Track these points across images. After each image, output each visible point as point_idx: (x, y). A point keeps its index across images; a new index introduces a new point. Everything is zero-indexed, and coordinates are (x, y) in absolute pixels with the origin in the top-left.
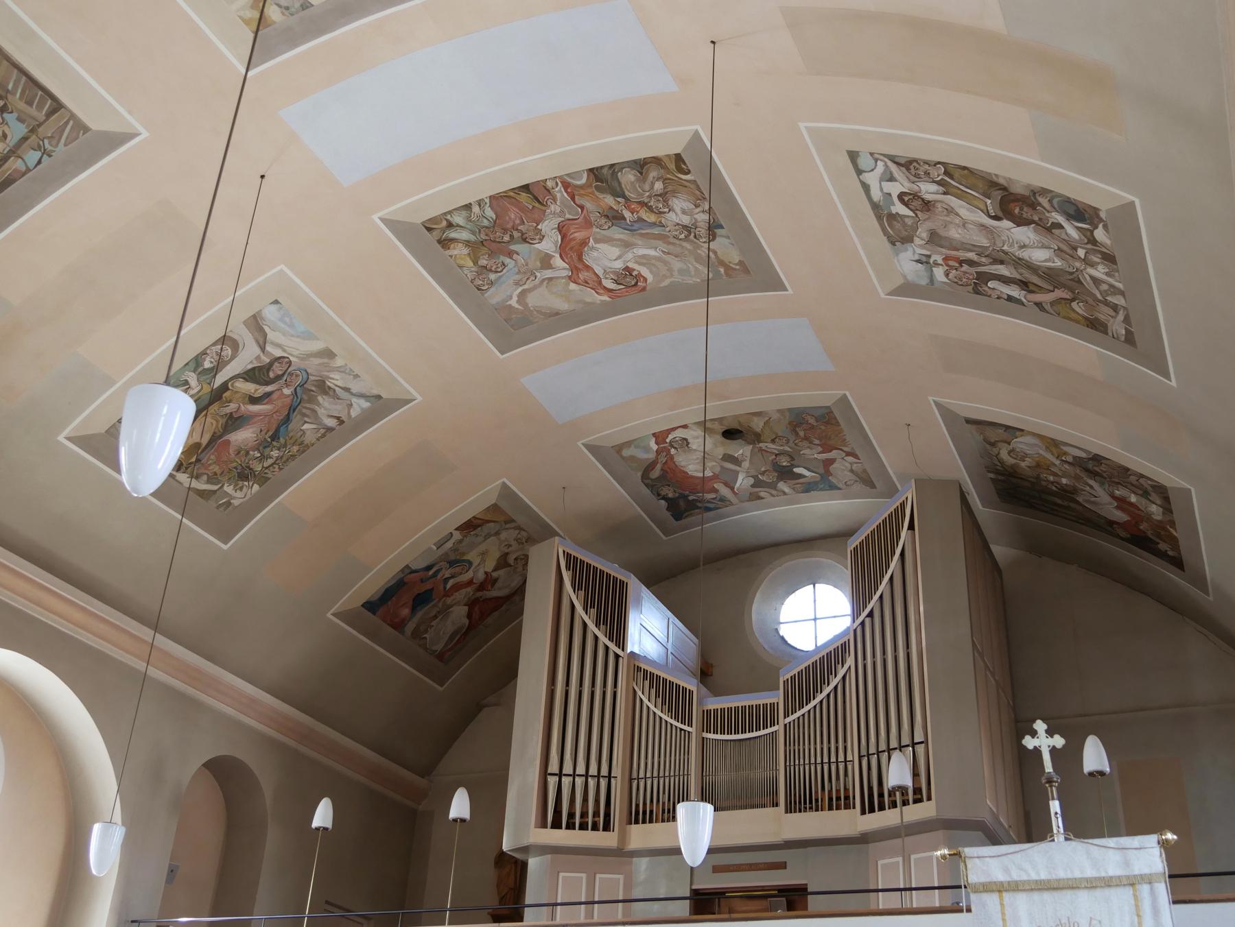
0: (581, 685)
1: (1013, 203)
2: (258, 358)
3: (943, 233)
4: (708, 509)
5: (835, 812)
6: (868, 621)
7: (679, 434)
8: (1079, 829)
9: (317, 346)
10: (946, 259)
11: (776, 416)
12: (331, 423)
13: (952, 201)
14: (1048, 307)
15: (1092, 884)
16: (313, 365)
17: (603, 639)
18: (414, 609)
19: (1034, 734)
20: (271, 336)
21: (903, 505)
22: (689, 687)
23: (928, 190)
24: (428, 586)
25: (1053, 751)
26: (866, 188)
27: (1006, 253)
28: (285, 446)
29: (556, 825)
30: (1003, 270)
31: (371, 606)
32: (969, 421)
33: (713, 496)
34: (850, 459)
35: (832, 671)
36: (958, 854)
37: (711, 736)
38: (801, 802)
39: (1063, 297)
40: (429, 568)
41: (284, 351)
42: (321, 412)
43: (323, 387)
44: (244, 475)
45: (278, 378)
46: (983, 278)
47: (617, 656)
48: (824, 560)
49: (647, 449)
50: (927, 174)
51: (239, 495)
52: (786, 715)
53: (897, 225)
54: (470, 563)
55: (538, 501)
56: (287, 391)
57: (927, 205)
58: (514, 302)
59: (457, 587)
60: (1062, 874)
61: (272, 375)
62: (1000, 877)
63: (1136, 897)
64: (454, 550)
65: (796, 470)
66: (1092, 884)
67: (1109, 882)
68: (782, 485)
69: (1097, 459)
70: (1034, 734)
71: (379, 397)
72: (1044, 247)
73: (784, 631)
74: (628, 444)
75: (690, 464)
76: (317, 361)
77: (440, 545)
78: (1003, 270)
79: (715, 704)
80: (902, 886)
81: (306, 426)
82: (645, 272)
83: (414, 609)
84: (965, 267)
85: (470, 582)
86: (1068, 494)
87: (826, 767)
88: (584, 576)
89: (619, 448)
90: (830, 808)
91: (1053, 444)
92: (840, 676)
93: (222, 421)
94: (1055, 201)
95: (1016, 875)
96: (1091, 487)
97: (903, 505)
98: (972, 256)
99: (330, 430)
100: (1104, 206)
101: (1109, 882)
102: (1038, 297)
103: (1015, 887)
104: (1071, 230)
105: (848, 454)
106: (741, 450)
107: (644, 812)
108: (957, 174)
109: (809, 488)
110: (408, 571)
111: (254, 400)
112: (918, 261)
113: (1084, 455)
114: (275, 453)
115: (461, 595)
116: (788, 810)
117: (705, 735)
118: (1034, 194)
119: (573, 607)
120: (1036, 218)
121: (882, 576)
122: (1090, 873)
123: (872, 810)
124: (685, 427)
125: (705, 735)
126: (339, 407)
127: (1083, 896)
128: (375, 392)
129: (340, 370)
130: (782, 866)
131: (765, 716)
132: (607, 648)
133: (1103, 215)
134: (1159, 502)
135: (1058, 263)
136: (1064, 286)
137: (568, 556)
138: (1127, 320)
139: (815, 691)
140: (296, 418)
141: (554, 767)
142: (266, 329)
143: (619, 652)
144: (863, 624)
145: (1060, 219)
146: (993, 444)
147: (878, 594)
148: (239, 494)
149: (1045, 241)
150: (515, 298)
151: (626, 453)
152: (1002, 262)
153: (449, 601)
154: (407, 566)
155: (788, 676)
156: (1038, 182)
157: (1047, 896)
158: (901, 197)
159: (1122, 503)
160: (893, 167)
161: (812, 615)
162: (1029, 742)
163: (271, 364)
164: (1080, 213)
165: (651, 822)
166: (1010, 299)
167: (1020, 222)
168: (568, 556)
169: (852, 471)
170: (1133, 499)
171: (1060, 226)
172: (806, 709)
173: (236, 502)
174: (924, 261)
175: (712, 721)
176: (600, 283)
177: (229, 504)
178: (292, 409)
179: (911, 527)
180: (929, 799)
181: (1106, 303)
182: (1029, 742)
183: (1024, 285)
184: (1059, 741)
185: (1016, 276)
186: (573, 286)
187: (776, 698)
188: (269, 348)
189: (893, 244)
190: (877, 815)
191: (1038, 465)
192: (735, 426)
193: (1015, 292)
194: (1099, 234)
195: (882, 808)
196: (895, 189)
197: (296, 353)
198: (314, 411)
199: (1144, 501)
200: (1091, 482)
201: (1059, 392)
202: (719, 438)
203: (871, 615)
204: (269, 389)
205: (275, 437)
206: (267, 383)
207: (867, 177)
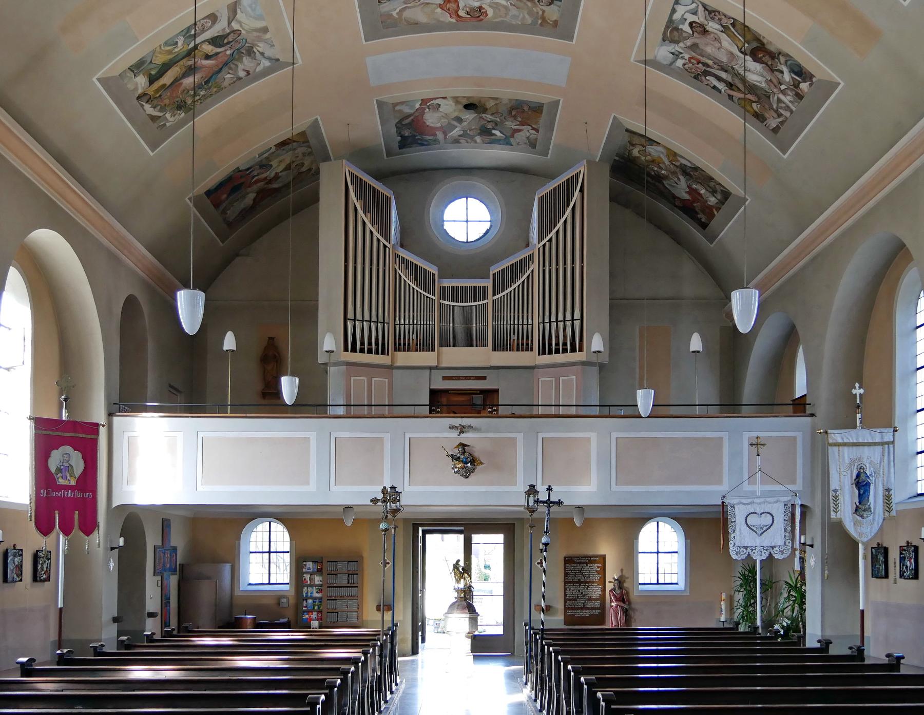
0: (355, 262)
1: (759, 50)
2: (224, 29)
3: (701, 46)
4: (422, 145)
5: (520, 352)
6: (548, 244)
7: (438, 101)
8: (866, 425)
9: (260, 24)
10: (690, 58)
11: (505, 102)
12: (242, 74)
13: (723, 36)
14: (735, 99)
15: (869, 444)
16: (251, 37)
17: (376, 234)
18: (229, 195)
19: (855, 388)
20: (240, 15)
21: (577, 175)
22: (432, 271)
23: (713, 26)
24: (242, 180)
25: (860, 395)
26: (674, 11)
27: (733, 68)
28: (210, 88)
29: (354, 350)
30: (723, 75)
31: (209, 193)
32: (627, 130)
33: (431, 138)
34: (534, 132)
35: (522, 272)
36: (826, 432)
37: (446, 302)
38: (501, 345)
39: (754, 103)
40: (248, 169)
41: (241, 26)
42: (241, 66)
43: (250, 52)
44: (181, 106)
45: (228, 43)
46: (706, 73)
47: (385, 247)
48: (479, 183)
49: (412, 107)
50: (720, 20)
51: (171, 118)
52: (494, 295)
53: (676, 33)
54: (271, 166)
55: (331, 133)
56: (228, 52)
57: (705, 32)
58: (395, 14)
59: (256, 182)
60: (861, 441)
61: (226, 41)
62: (840, 441)
63: (883, 450)
64: (267, 158)
65: (493, 132)
66: (869, 444)
67: (875, 444)
68: (478, 139)
69: (696, 169)
70: (855, 388)
71: (278, 60)
72: (762, 76)
73: (447, 226)
74: (402, 103)
75: (431, 119)
76: (255, 34)
77: (260, 155)
78: (723, 75)
79: (448, 283)
80: (846, 449)
81: (229, 76)
82: (490, 12)
83: (229, 195)
84: (700, 65)
85: (266, 178)
86: (659, 178)
87: (520, 327)
88: (362, 189)
89: (395, 105)
90: (518, 350)
91: (673, 155)
92: (526, 275)
93: (184, 70)
94: (789, 63)
95: (846, 441)
96: (679, 179)
97: (577, 175)
98: (710, 62)
99: (240, 79)
100: (818, 75)
101: (875, 444)
102: (731, 93)
103: (845, 444)
104: (787, 77)
105: (533, 129)
106: (469, 116)
107: (404, 344)
108: (738, 26)
109: (497, 141)
110: (238, 170)
111: (207, 57)
112: (673, 54)
113: (689, 165)
114: (202, 93)
115: (255, 187)
116: (494, 350)
117: (442, 301)
118: (780, 53)
119: (356, 209)
120: (769, 63)
121: (560, 218)
122: (870, 441)
123: (544, 353)
124: (444, 98)
125: (442, 301)
126: (252, 65)
127: (866, 448)
128: (277, 57)
129: (266, 41)
130: (484, 378)
131: (481, 293)
132: (378, 240)
133: (814, 80)
134: (719, 197)
135: (763, 85)
136: (756, 95)
137: (352, 175)
138: (782, 123)
139: (512, 282)
140: (225, 69)
141: (350, 315)
142: (239, 11)
143: (387, 244)
144: (544, 246)
145: (785, 70)
146: (632, 144)
147: (556, 229)
148: (172, 119)
149: (765, 73)
150: (398, 10)
151: (397, 108)
152: (726, 71)
153: (249, 189)
154: (238, 168)
155: (496, 271)
156: (786, 50)
157: (854, 448)
158: (691, 24)
159: (692, 191)
160: (701, 8)
161: (466, 219)
162: (854, 391)
163: (229, 34)
164: (800, 72)
165: (409, 350)
166: (714, 87)
167: (756, 59)
168: (352, 175)
169: (528, 138)
170: (703, 191)
171: (782, 72)
172: (506, 292)
173: (168, 124)
174: (676, 55)
175: (446, 293)
176: (457, 12)
177: (165, 125)
178: (226, 64)
179: (581, 190)
180: (581, 350)
181: (776, 111)
182: (854, 391)
183: (730, 85)
184: (862, 391)
185: (730, 80)
186: (439, 10)
187: (488, 283)
188: (233, 24)
189: (664, 40)
190: (547, 357)
191: (653, 161)
192: (471, 101)
193: (721, 86)
194: (804, 86)
195: (550, 353)
196: (691, 18)
197: (247, 27)
198: (237, 66)
199: (708, 194)
200: (681, 177)
201: (698, 130)
202: (461, 107)
203: (550, 240)
204: (219, 50)
205: (206, 83)
206: (221, 46)
207: (678, 8)
